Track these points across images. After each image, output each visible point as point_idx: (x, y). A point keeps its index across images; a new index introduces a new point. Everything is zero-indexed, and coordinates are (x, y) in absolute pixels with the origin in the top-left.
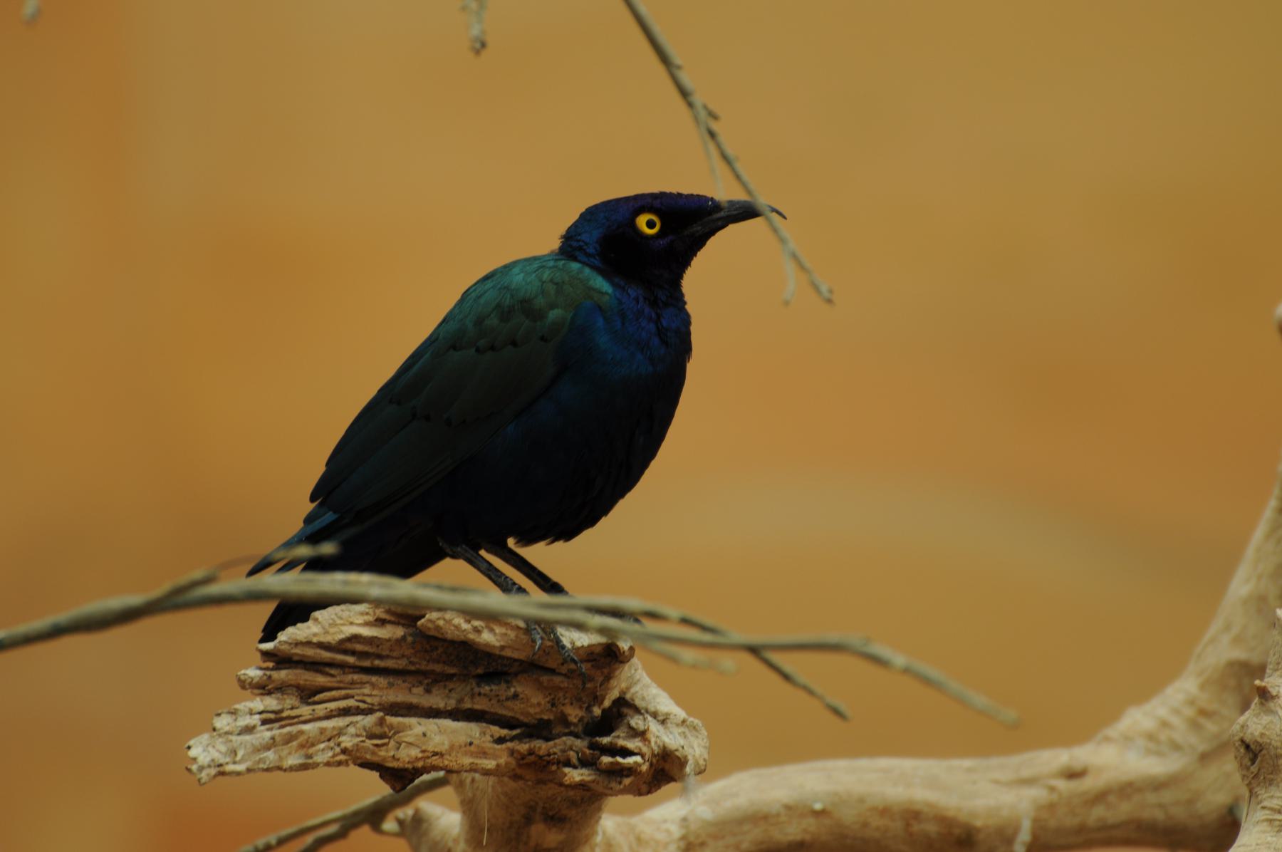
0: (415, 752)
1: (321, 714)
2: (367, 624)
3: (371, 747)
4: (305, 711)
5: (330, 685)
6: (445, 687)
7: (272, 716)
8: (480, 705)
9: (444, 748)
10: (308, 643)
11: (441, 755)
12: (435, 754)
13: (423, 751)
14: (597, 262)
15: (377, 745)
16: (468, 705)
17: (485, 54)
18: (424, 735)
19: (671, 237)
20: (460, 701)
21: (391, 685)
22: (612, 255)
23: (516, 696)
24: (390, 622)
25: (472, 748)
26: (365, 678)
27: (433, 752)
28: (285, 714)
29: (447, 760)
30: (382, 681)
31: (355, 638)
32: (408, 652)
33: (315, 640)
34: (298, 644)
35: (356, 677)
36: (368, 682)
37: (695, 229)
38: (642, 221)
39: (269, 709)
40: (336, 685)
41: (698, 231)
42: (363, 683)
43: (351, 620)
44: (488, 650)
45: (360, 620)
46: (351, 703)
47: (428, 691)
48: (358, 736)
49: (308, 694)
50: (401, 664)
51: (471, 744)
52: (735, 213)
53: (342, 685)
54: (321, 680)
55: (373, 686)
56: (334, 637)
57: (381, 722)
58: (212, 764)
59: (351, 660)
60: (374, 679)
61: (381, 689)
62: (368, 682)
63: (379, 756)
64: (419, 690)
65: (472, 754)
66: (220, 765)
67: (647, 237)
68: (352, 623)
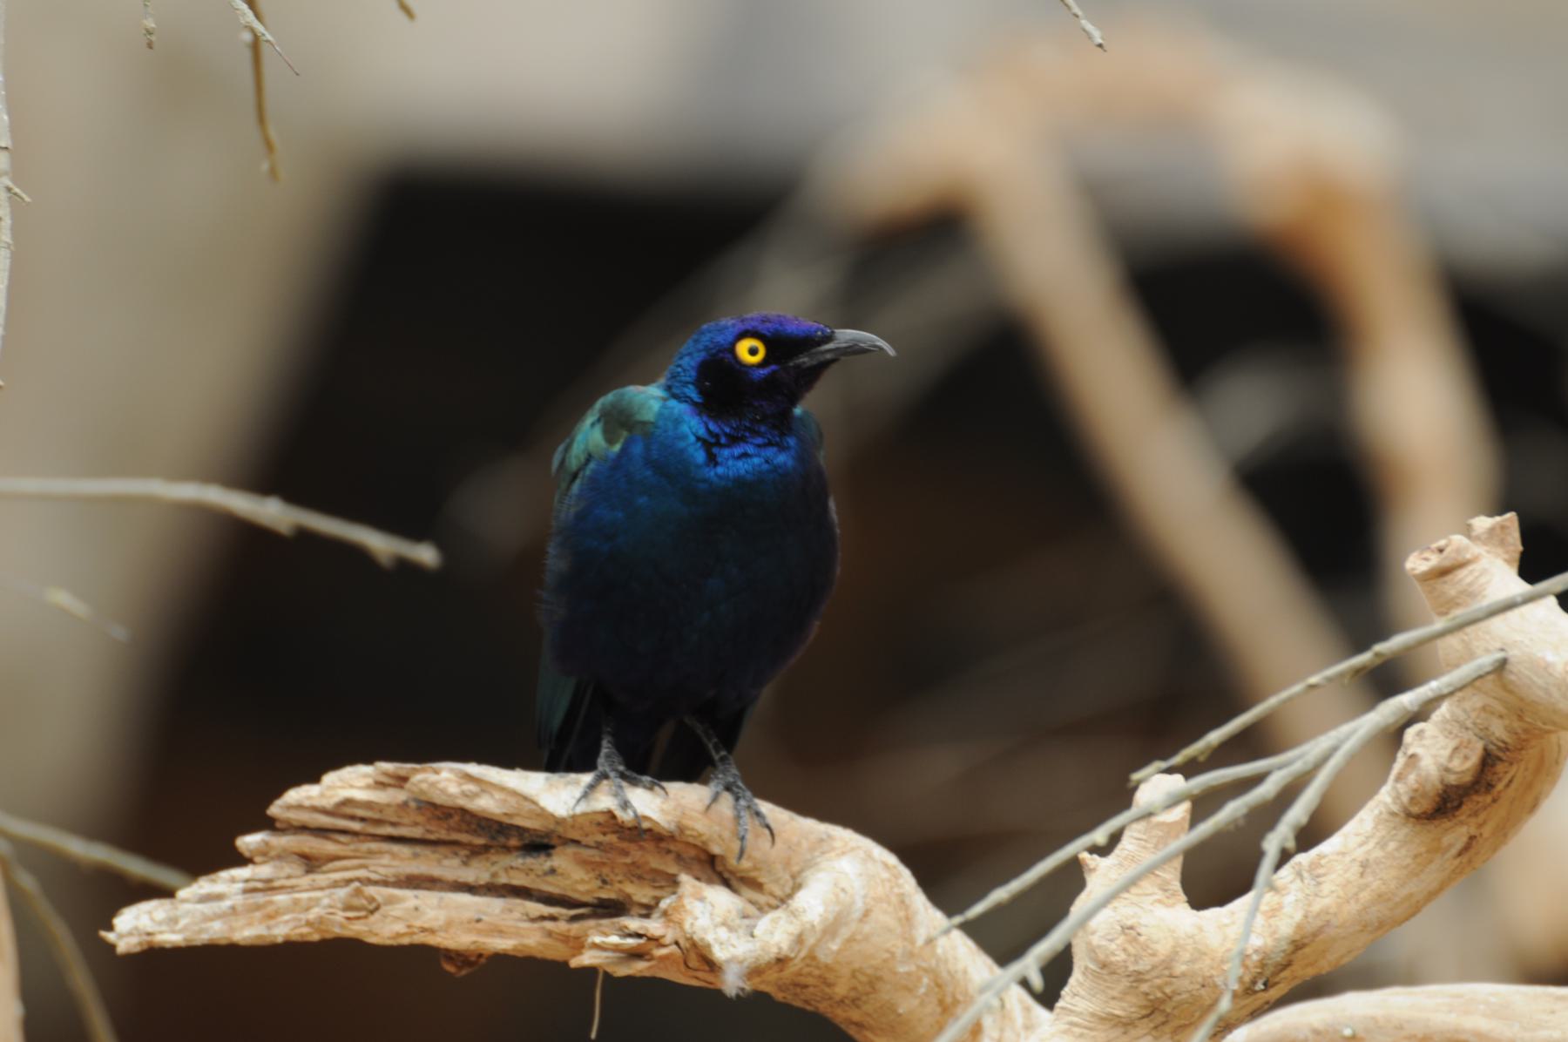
0: (400, 927)
1: (324, 884)
2: (368, 787)
3: (343, 921)
4: (306, 881)
5: (342, 853)
6: (487, 859)
7: (260, 885)
8: (519, 880)
9: (435, 925)
10: (315, 809)
11: (432, 931)
12: (424, 930)
13: (409, 927)
14: (692, 392)
15: (348, 919)
16: (503, 879)
17: (1106, 47)
18: (416, 909)
19: (773, 367)
20: (494, 875)
21: (416, 856)
22: (707, 384)
23: (553, 871)
24: (390, 785)
25: (479, 926)
26: (385, 846)
27: (422, 928)
28: (277, 884)
29: (440, 937)
30: (404, 850)
31: (348, 802)
32: (420, 819)
33: (307, 803)
34: (300, 807)
35: (374, 846)
36: (387, 852)
37: (801, 360)
38: (743, 348)
39: (257, 877)
40: (352, 854)
41: (804, 363)
42: (381, 853)
43: (352, 783)
44: (486, 815)
45: (362, 782)
46: (361, 873)
47: (465, 864)
48: (331, 907)
49: (311, 863)
50: (417, 832)
51: (479, 921)
52: (844, 345)
53: (358, 854)
54: (329, 847)
55: (394, 856)
56: (328, 803)
57: (358, 892)
58: (135, 932)
59: (356, 826)
60: (396, 848)
61: (402, 859)
62: (387, 852)
63: (351, 930)
64: (456, 862)
65: (479, 932)
66: (149, 934)
67: (752, 366)
68: (352, 787)
